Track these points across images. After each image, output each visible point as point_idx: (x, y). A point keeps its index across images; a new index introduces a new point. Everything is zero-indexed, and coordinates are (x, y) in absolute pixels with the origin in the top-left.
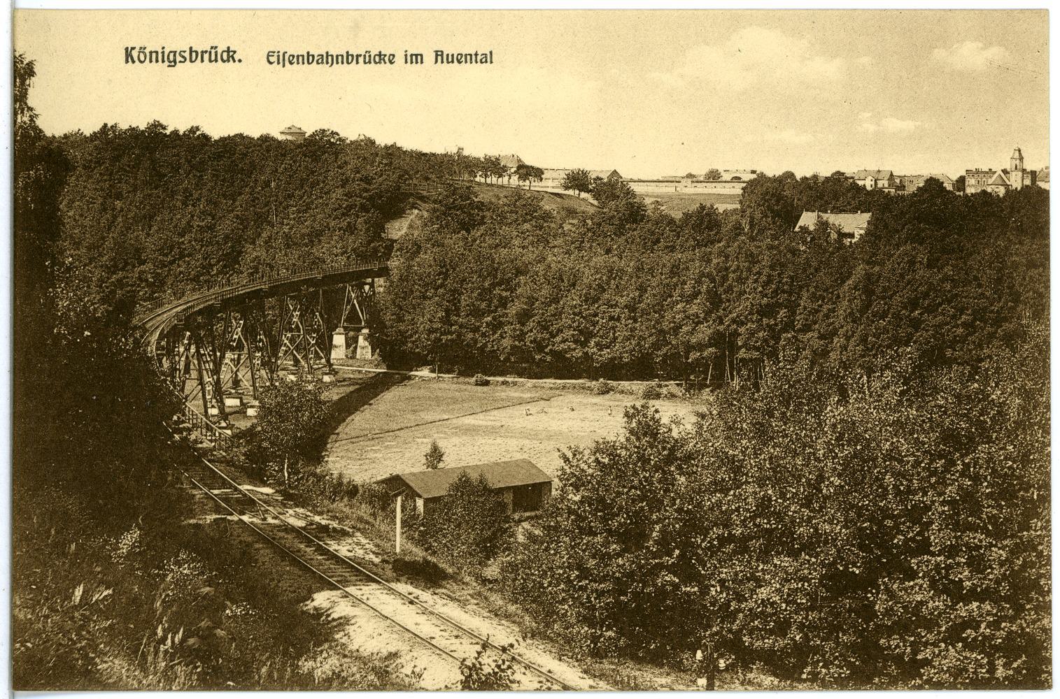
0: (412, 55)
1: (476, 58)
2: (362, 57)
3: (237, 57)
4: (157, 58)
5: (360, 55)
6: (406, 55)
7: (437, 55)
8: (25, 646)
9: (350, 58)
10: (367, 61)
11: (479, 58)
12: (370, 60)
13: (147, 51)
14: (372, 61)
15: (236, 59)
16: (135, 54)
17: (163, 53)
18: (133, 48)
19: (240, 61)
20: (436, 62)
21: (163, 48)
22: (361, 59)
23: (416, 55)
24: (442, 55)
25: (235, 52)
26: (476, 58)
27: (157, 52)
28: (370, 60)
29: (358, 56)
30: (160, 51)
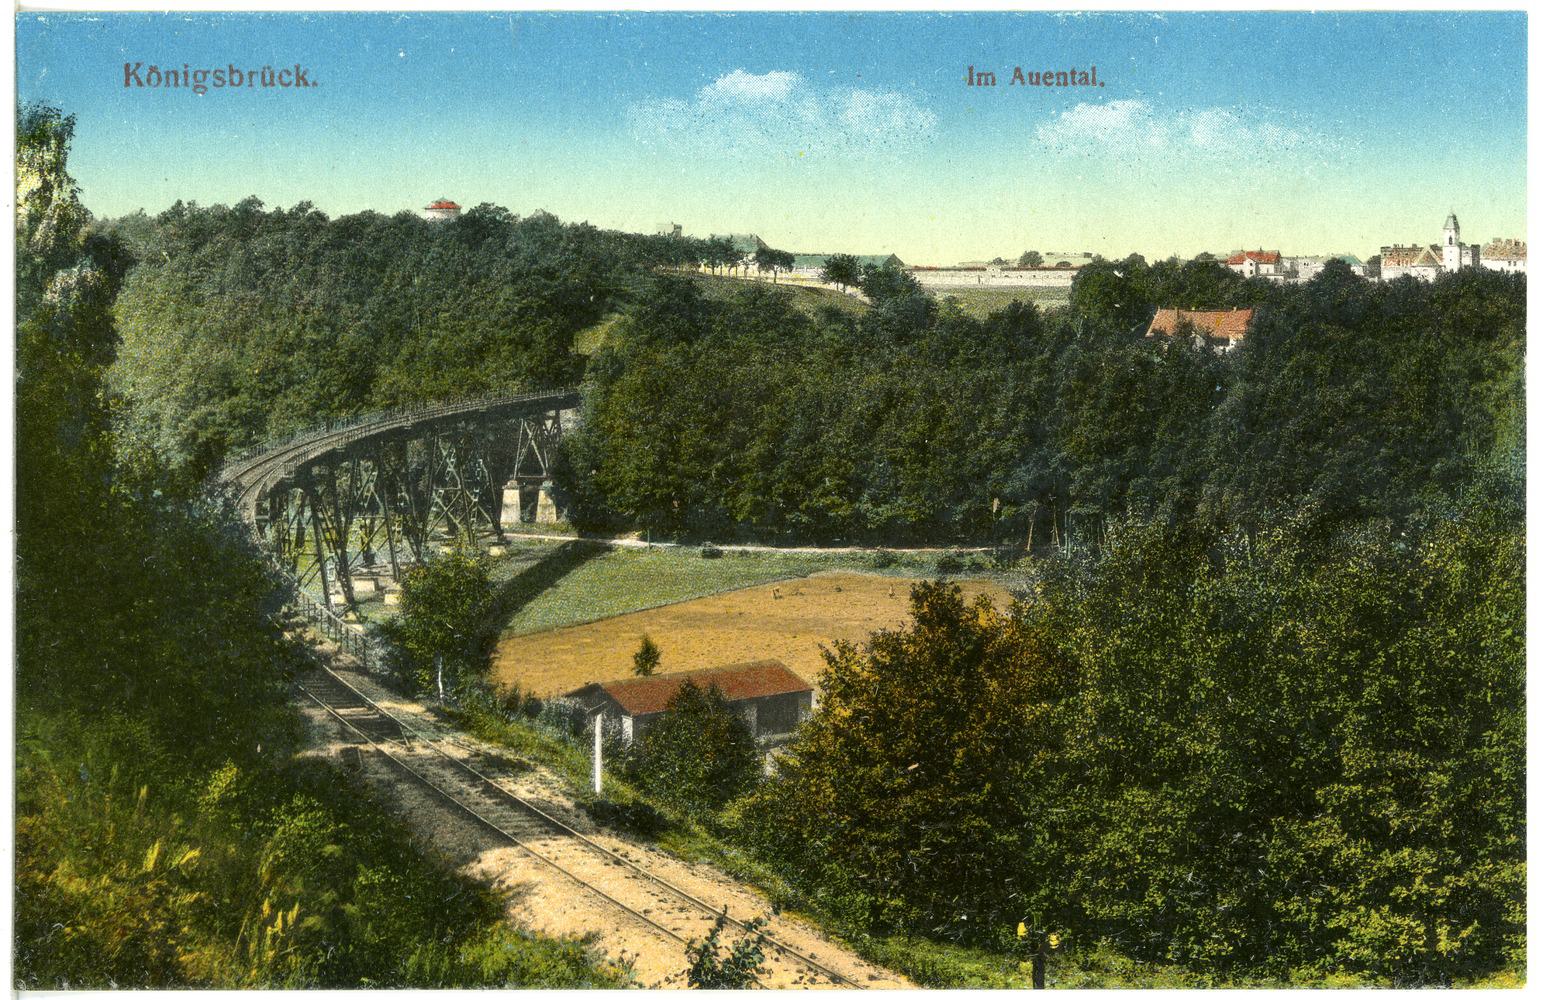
1: (1073, 78)
3: (310, 79)
16: (143, 73)
17: (186, 73)
18: (138, 65)
20: (127, 84)
23: (987, 75)
26: (1073, 78)
28: (167, 78)
29: (251, 74)
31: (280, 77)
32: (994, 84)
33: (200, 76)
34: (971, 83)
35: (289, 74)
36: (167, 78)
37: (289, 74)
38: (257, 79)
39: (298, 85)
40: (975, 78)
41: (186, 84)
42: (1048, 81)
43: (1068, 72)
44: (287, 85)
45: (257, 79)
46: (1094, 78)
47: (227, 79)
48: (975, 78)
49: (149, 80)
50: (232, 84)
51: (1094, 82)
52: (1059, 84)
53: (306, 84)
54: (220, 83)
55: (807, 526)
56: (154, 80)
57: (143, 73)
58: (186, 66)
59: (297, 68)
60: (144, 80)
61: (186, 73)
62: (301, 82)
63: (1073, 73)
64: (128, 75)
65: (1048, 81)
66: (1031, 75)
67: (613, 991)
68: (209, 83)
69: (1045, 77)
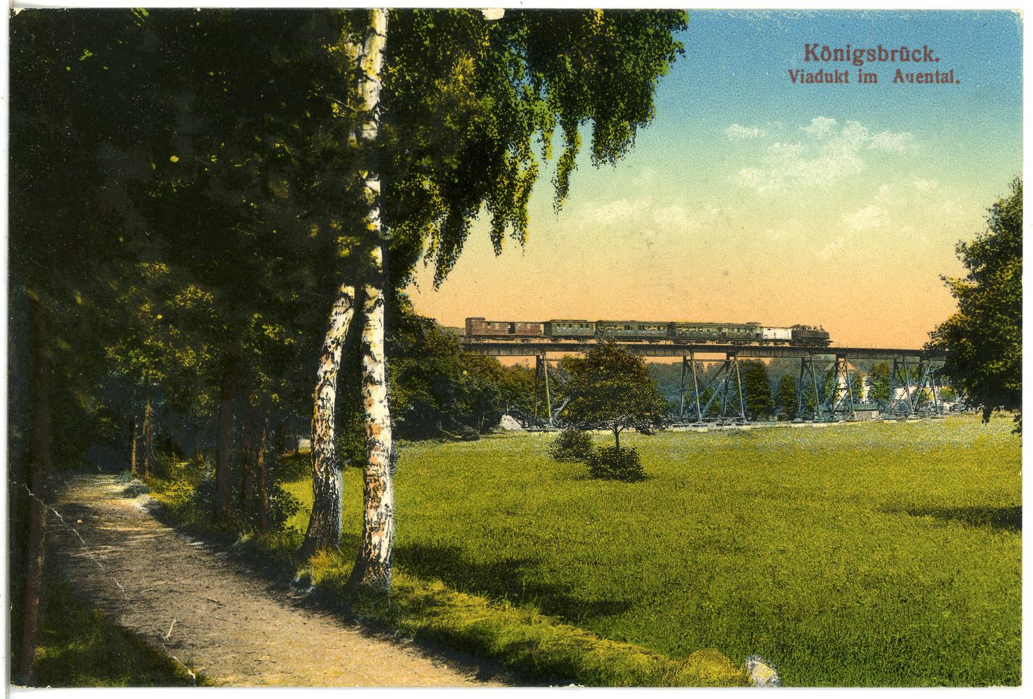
0: (866, 75)
1: (937, 78)
3: (933, 56)
4: (842, 56)
5: (897, 51)
6: (811, 79)
8: (572, 41)
10: (905, 57)
11: (940, 77)
12: (908, 56)
14: (911, 58)
15: (934, 58)
16: (818, 51)
17: (848, 52)
18: (816, 45)
19: (937, 60)
21: (848, 46)
23: (871, 75)
26: (937, 78)
27: (841, 51)
28: (908, 56)
29: (893, 52)
30: (845, 48)
31: (913, 55)
32: (876, 82)
33: (858, 54)
34: (860, 81)
35: (919, 52)
37: (919, 52)
38: (897, 55)
39: (925, 60)
40: (863, 77)
41: (848, 59)
42: (920, 79)
43: (934, 73)
44: (918, 60)
45: (897, 55)
46: (952, 77)
47: (877, 56)
48: (863, 77)
49: (822, 55)
50: (880, 59)
51: (952, 81)
52: (927, 82)
53: (931, 60)
54: (871, 58)
55: (128, 536)
56: (826, 56)
57: (818, 51)
58: (848, 46)
59: (925, 47)
60: (819, 56)
61: (848, 52)
62: (928, 59)
63: (937, 74)
64: (808, 52)
65: (920, 79)
66: (907, 75)
67: (1024, 623)
68: (864, 58)
69: (918, 77)
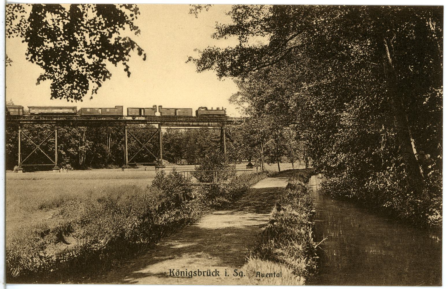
2: (206, 272)
7: (257, 274)
9: (200, 273)
13: (180, 271)
18: (174, 270)
22: (205, 274)
24: (259, 274)
25: (219, 272)
28: (204, 274)
36: (204, 274)
